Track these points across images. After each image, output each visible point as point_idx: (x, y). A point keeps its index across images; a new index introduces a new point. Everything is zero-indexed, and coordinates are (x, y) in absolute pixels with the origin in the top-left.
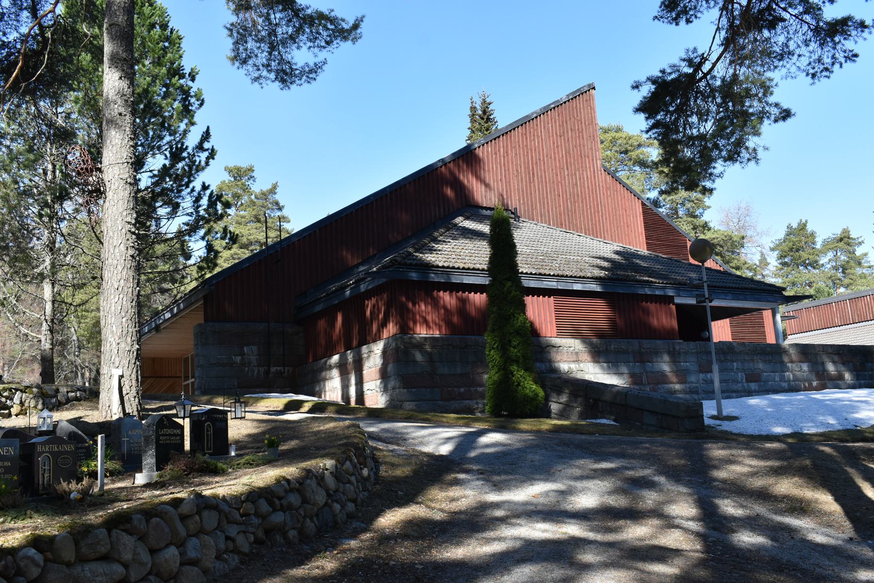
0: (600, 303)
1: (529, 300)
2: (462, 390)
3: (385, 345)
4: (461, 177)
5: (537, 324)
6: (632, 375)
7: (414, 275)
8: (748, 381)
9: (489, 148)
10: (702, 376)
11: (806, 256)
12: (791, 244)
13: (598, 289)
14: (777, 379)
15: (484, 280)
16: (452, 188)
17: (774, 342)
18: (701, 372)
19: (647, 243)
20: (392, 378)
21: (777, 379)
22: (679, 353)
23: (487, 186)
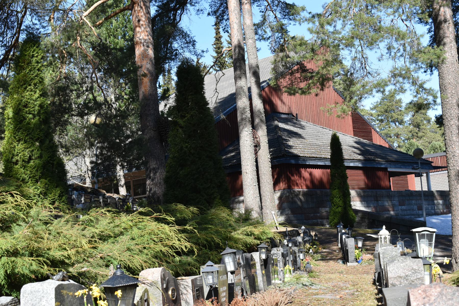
0: (360, 172)
1: (348, 172)
2: (312, 215)
3: (281, 194)
4: (272, 99)
5: (244, 187)
6: (374, 207)
7: (293, 162)
8: (418, 210)
9: (334, 95)
10: (400, 207)
11: (396, 116)
12: (386, 107)
13: (360, 165)
14: (430, 209)
15: (328, 163)
16: (268, 105)
17: (427, 190)
18: (400, 205)
19: (354, 131)
20: (286, 210)
21: (430, 209)
22: (391, 196)
23: (284, 103)
